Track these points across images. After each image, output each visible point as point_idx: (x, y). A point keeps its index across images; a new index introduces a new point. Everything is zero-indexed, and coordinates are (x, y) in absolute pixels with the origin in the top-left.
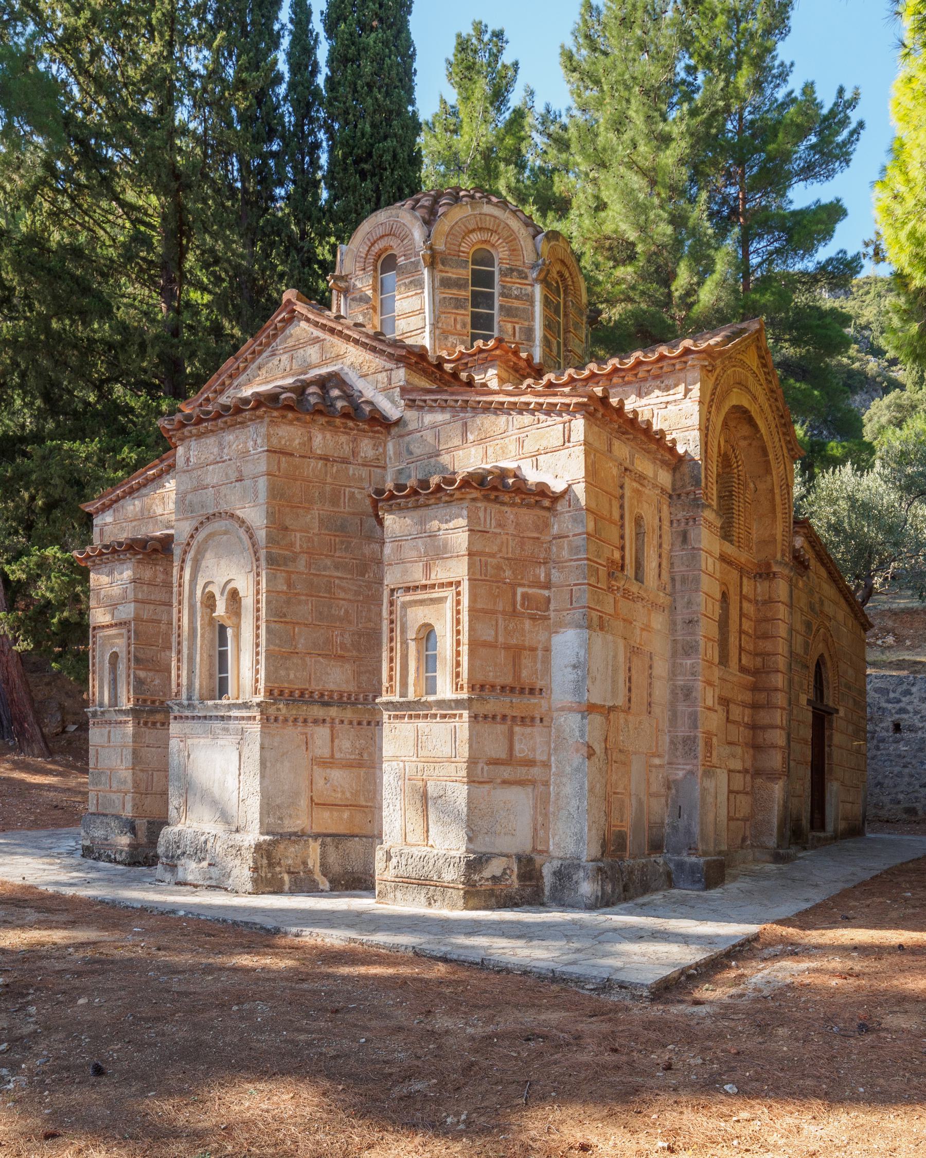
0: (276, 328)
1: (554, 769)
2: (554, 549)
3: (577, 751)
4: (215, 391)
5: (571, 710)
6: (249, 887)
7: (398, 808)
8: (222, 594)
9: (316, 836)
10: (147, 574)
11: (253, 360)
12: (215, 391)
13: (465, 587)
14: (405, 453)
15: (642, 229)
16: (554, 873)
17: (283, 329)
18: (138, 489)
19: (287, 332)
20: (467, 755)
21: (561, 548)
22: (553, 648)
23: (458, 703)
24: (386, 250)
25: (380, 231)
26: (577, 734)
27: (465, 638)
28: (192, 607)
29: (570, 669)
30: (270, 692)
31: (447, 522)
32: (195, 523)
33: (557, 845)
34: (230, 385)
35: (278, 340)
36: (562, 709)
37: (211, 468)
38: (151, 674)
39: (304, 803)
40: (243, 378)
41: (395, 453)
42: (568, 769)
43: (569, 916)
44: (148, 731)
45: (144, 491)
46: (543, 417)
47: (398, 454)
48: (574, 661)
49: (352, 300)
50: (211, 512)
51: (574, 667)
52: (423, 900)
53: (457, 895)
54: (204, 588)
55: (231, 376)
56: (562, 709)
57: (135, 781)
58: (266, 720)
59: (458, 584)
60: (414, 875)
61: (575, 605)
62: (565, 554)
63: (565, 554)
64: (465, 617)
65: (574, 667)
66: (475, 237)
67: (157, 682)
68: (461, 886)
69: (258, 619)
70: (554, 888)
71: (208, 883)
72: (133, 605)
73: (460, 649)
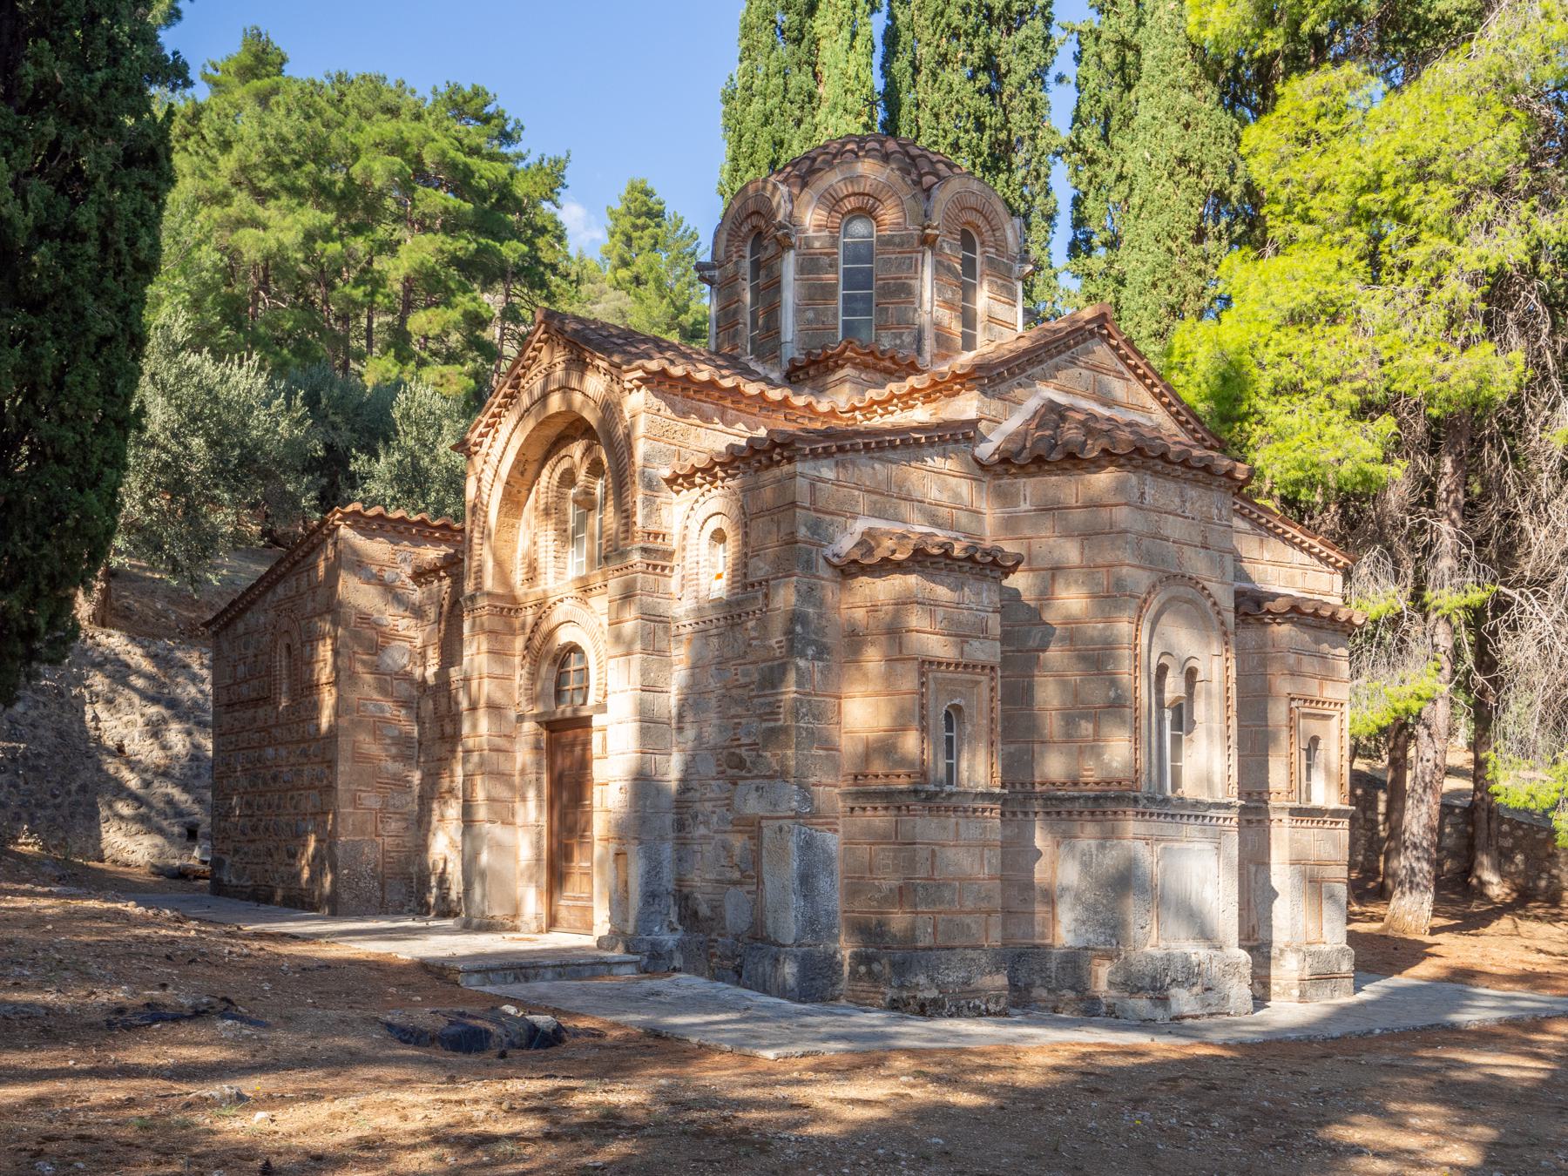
25: (972, 201)
45: (891, 455)
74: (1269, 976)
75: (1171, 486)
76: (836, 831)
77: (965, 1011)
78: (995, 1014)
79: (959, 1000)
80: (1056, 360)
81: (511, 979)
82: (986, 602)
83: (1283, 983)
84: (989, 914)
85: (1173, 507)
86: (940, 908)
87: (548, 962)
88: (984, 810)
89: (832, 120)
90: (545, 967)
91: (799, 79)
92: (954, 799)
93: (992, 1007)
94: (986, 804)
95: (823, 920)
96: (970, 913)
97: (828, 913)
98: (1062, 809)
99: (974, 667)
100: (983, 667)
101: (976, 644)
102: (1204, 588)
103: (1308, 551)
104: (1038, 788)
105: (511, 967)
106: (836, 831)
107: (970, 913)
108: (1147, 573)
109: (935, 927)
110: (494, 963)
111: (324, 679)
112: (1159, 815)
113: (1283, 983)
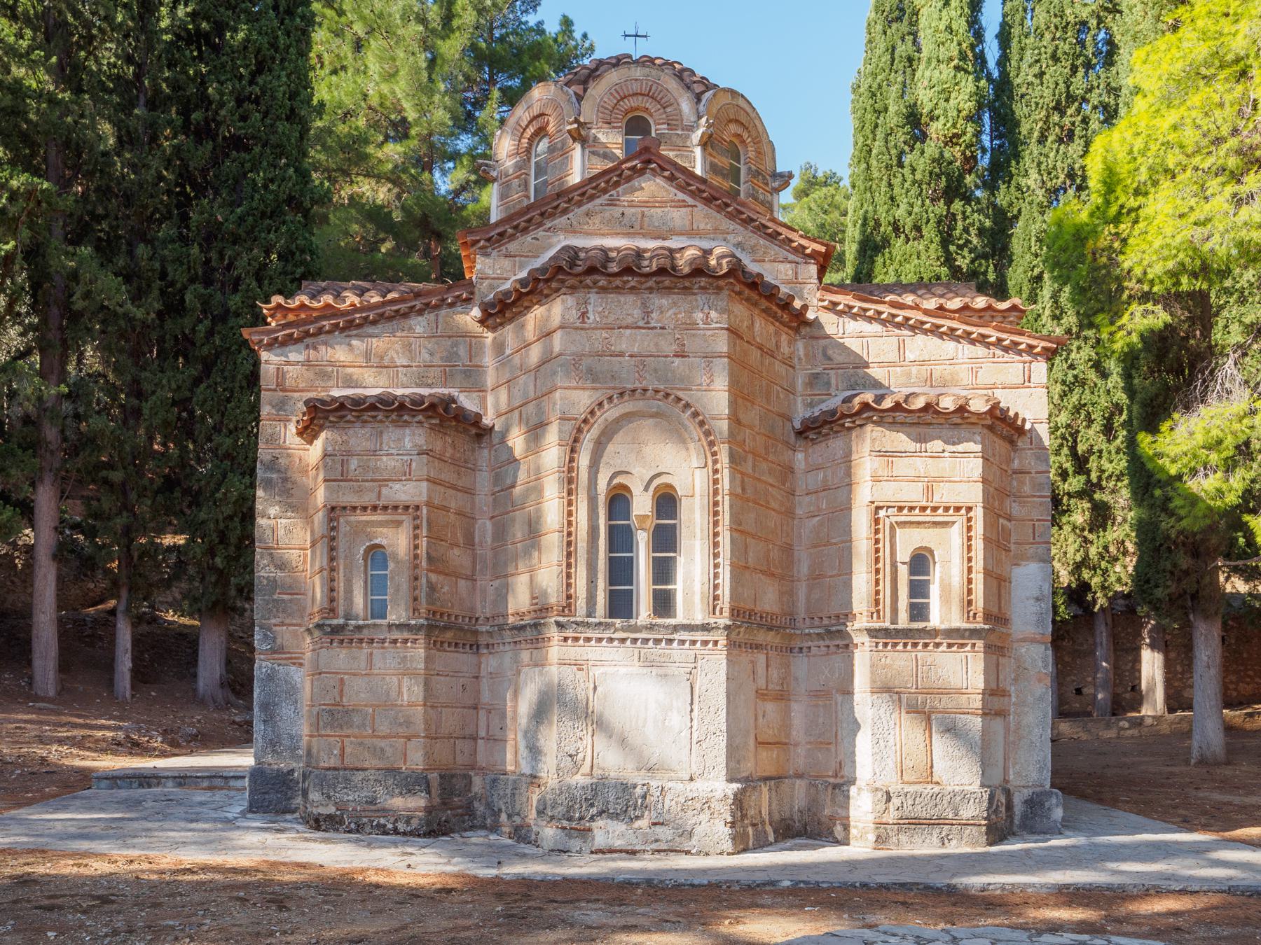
0: (620, 175)
1: (1014, 699)
2: (1015, 483)
3: (1040, 681)
4: (515, 228)
5: (1033, 641)
6: (728, 846)
7: (891, 742)
8: (646, 489)
9: (766, 779)
10: (438, 446)
11: (580, 204)
12: (515, 228)
13: (978, 513)
14: (820, 356)
15: (423, 112)
16: (1026, 802)
17: (629, 179)
18: (359, 326)
19: (635, 183)
20: (982, 686)
21: (1022, 483)
22: (1013, 580)
23: (974, 633)
24: (637, 109)
25: (636, 87)
26: (1040, 664)
27: (978, 564)
28: (592, 501)
29: (1032, 602)
30: (736, 612)
31: (954, 444)
32: (598, 395)
33: (1018, 774)
34: (540, 225)
35: (619, 189)
36: (1024, 640)
37: (628, 332)
38: (441, 578)
39: (752, 742)
40: (561, 221)
41: (806, 355)
42: (1030, 699)
43: (333, 855)
44: (438, 653)
45: (370, 330)
46: (999, 352)
47: (810, 357)
48: (1036, 593)
49: (593, 153)
50: (630, 386)
51: (1037, 599)
52: (935, 840)
53: (979, 833)
54: (611, 479)
55: (542, 214)
56: (1024, 640)
57: (426, 722)
58: (732, 645)
59: (969, 509)
60: (924, 815)
61: (1037, 539)
62: (1027, 489)
63: (1027, 489)
64: (978, 545)
65: (1037, 599)
66: (733, 128)
67: (446, 589)
68: (983, 822)
69: (716, 524)
70: (1025, 817)
71: (654, 846)
72: (425, 484)
73: (973, 576)
74: (848, 817)
75: (630, 298)
76: (301, 665)
77: (368, 829)
78: (405, 834)
79: (360, 817)
80: (589, 206)
81: (136, 785)
82: (408, 445)
83: (860, 825)
84: (409, 738)
85: (630, 320)
86: (349, 732)
87: (167, 774)
88: (406, 641)
89: (927, 74)
90: (167, 778)
91: (903, 49)
92: (365, 631)
93: (401, 827)
94: (406, 635)
95: (286, 742)
96: (384, 737)
97: (291, 737)
98: (676, 636)
99: (396, 508)
100: (407, 508)
101: (397, 486)
102: (679, 399)
103: (982, 340)
104: (511, 620)
105: (134, 776)
106: (301, 665)
107: (384, 737)
108: (587, 393)
109: (342, 749)
110: (118, 773)
111: (804, 584)
112: (600, 640)
113: (860, 825)
